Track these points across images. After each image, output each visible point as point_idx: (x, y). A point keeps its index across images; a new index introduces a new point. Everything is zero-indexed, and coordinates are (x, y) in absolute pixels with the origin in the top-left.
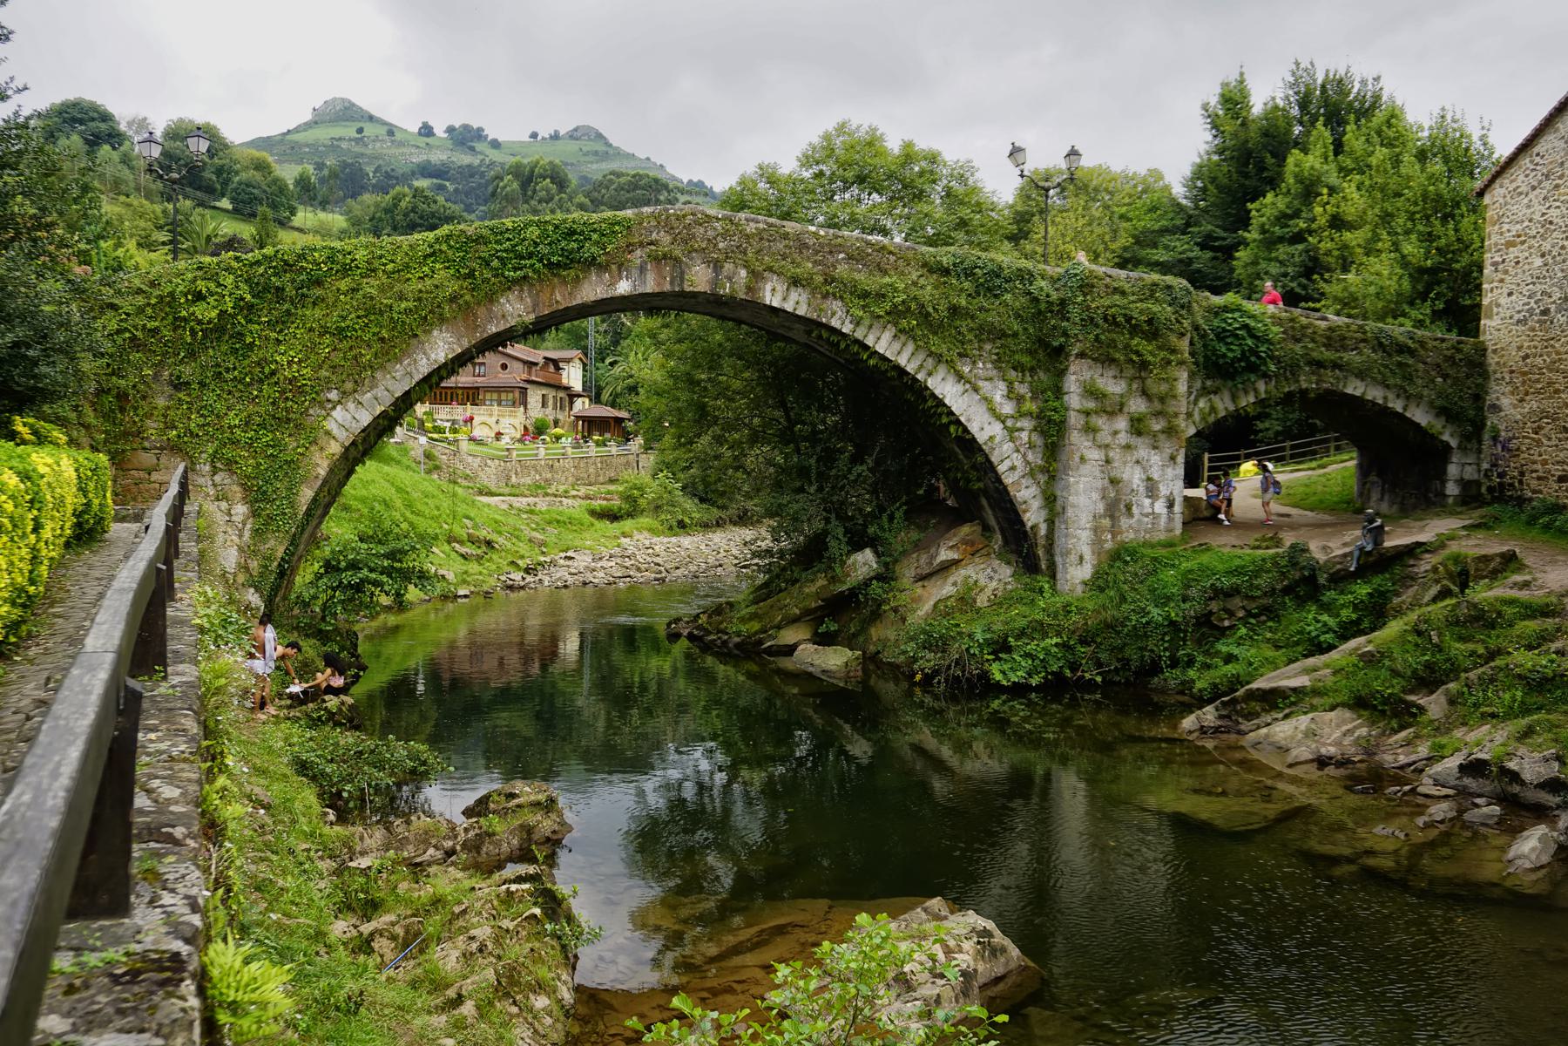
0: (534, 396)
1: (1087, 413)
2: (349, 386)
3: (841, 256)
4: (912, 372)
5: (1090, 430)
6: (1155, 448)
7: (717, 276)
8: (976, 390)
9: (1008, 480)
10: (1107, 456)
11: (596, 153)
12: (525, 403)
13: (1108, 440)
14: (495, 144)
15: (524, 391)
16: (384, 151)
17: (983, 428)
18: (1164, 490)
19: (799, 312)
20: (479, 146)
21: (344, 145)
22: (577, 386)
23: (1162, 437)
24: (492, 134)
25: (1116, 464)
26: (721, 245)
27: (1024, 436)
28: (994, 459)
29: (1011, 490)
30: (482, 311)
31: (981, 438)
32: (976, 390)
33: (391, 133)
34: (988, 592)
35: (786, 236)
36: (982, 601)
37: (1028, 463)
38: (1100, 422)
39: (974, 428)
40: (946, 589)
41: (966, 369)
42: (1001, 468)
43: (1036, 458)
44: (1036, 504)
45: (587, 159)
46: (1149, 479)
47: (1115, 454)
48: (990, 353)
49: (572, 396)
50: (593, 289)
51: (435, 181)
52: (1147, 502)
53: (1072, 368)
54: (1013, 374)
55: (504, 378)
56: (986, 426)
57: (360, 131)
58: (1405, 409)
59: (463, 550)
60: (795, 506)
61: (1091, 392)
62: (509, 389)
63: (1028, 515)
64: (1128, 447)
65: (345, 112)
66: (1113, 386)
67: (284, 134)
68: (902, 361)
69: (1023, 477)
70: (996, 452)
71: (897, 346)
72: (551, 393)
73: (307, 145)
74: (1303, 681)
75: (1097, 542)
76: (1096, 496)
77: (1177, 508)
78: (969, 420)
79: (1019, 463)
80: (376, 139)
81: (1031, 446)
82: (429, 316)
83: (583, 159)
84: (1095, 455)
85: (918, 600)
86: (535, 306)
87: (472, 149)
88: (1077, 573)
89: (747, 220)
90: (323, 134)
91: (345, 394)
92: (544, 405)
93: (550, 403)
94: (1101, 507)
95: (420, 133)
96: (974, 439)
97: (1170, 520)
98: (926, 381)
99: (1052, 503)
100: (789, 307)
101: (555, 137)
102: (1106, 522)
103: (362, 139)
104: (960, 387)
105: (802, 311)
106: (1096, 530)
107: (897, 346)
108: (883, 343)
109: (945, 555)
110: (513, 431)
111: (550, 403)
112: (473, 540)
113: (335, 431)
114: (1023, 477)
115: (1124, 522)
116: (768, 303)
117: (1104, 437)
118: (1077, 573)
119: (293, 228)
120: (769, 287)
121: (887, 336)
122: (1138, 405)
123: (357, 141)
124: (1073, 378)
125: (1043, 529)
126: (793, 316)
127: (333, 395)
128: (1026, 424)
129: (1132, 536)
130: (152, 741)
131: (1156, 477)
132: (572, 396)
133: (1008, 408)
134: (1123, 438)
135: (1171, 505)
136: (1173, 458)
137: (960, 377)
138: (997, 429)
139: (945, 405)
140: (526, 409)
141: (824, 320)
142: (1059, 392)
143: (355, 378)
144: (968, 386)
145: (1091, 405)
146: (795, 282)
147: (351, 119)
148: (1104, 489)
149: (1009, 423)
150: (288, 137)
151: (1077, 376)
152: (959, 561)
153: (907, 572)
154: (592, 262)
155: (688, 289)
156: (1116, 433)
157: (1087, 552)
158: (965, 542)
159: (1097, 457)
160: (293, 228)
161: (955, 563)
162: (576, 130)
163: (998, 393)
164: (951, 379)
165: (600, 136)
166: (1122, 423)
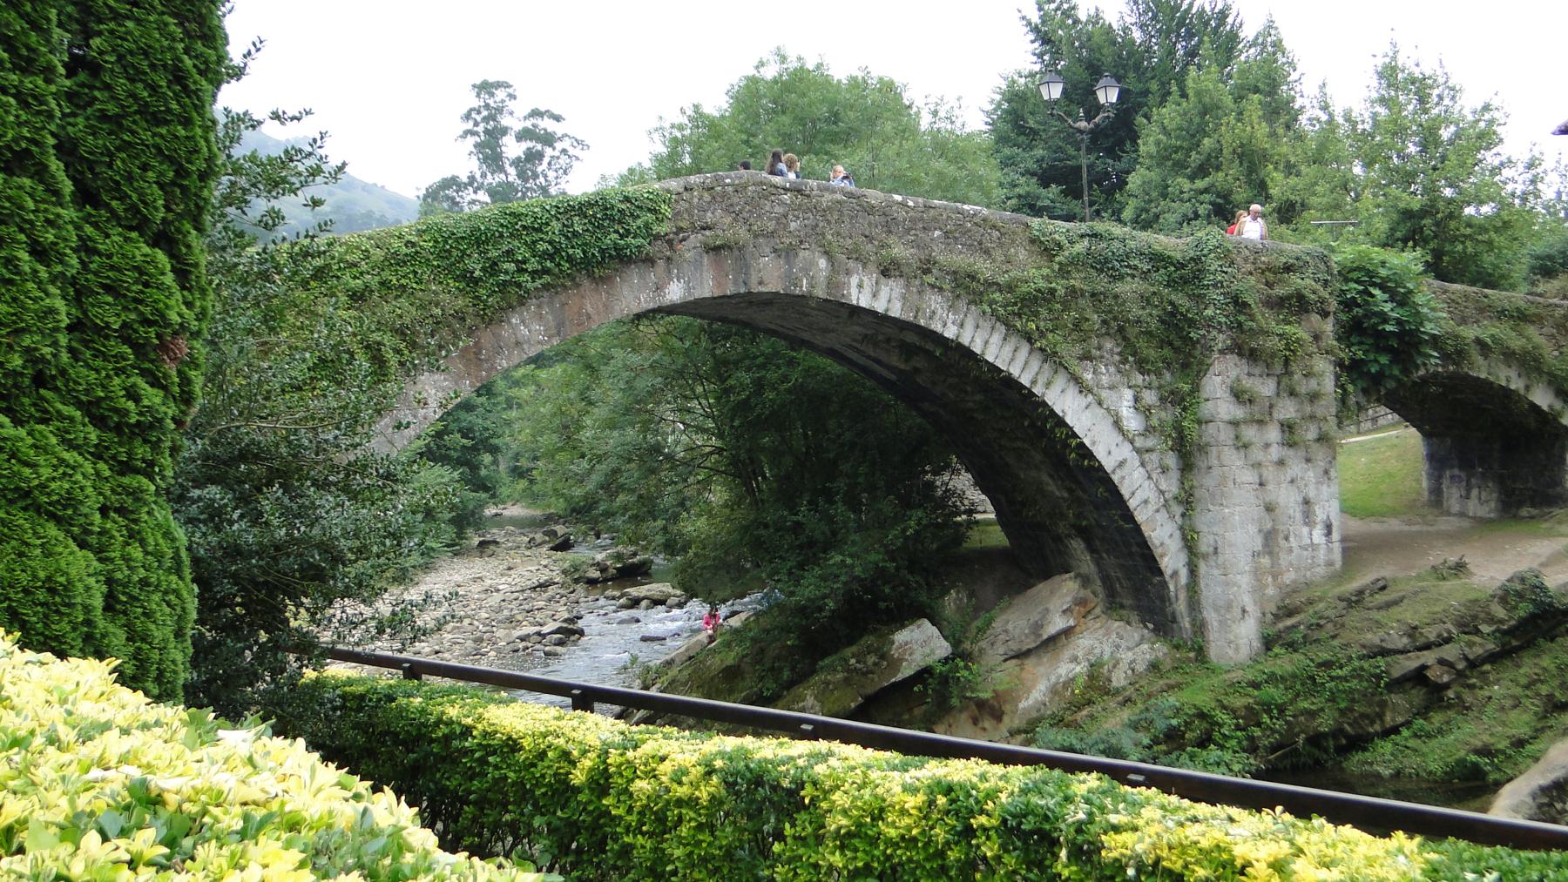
1: (1235, 424)
3: (937, 233)
4: (1028, 385)
6: (1308, 460)
7: (791, 268)
9: (1140, 517)
10: (1261, 477)
17: (1108, 449)
18: (1320, 514)
19: (893, 314)
23: (1315, 446)
25: (1270, 487)
26: (793, 226)
28: (1125, 492)
29: (1145, 529)
31: (1108, 464)
34: (1123, 666)
35: (870, 210)
37: (1162, 492)
38: (1249, 433)
39: (1100, 453)
40: (1068, 667)
42: (1132, 504)
43: (1171, 485)
47: (1269, 473)
48: (1111, 352)
52: (1305, 530)
53: (1217, 367)
56: (1113, 448)
58: (1527, 388)
60: (349, 543)
63: (1166, 559)
64: (1281, 463)
68: (1015, 371)
69: (1158, 511)
70: (1126, 482)
71: (1008, 350)
75: (1258, 589)
76: (1253, 529)
78: (1094, 443)
81: (1164, 470)
84: (1249, 476)
86: (560, 326)
89: (819, 189)
94: (1258, 543)
96: (1101, 468)
97: (1330, 550)
98: (1044, 394)
104: (1083, 401)
105: (896, 311)
106: (1257, 573)
107: (1008, 350)
114: (1158, 511)
115: (1284, 559)
116: (855, 302)
120: (854, 280)
121: (996, 339)
124: (1218, 379)
126: (884, 319)
131: (1312, 494)
133: (1133, 422)
134: (1275, 452)
135: (1329, 529)
137: (1083, 388)
138: (1126, 451)
139: (1066, 425)
141: (922, 322)
144: (1090, 397)
148: (1260, 520)
149: (1139, 442)
153: (992, 653)
155: (756, 289)
156: (1267, 446)
157: (1247, 601)
159: (1250, 479)
161: (1067, 632)
164: (1072, 391)
166: (1273, 434)
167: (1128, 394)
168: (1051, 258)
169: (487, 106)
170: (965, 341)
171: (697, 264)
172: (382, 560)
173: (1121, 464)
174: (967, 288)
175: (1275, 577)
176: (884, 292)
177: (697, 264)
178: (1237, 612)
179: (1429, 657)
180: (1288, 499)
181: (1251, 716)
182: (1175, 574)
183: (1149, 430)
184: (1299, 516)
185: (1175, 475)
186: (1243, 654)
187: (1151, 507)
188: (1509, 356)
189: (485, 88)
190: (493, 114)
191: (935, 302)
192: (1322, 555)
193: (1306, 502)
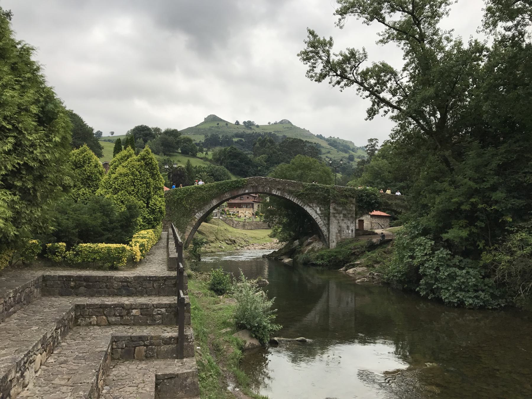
1: (334, 213)
2: (199, 210)
5: (334, 217)
11: (288, 128)
14: (258, 126)
15: (253, 204)
16: (225, 130)
17: (314, 215)
18: (351, 228)
20: (252, 127)
21: (213, 128)
24: (257, 123)
30: (222, 196)
33: (227, 124)
34: (317, 248)
35: (276, 181)
36: (316, 250)
38: (337, 215)
41: (311, 205)
43: (326, 222)
44: (326, 231)
47: (340, 221)
50: (241, 192)
51: (240, 139)
52: (347, 231)
55: (248, 201)
57: (218, 124)
59: (227, 242)
62: (249, 204)
64: (343, 220)
65: (213, 119)
67: (196, 126)
73: (203, 129)
74: (359, 262)
75: (337, 238)
77: (354, 232)
80: (223, 127)
81: (325, 220)
82: (212, 198)
84: (336, 221)
85: (305, 250)
87: (251, 128)
88: (333, 245)
90: (207, 126)
94: (337, 232)
95: (235, 124)
97: (352, 234)
99: (329, 231)
100: (277, 194)
101: (276, 123)
105: (279, 195)
106: (337, 236)
107: (298, 201)
108: (295, 201)
109: (309, 241)
110: (249, 214)
112: (230, 240)
113: (197, 217)
115: (342, 235)
117: (338, 218)
118: (333, 245)
119: (197, 157)
123: (217, 127)
133: (319, 212)
134: (342, 218)
135: (352, 231)
136: (352, 222)
137: (310, 207)
138: (318, 216)
140: (253, 208)
142: (329, 209)
143: (200, 209)
146: (279, 189)
147: (216, 121)
154: (241, 187)
158: (314, 238)
160: (197, 157)
162: (282, 121)
165: (289, 122)
166: (342, 215)
167: (318, 208)
168: (304, 188)
169: (372, 144)
170: (290, 199)
171: (250, 188)
172: (160, 199)
173: (317, 218)
174: (290, 193)
175: (340, 237)
176: (278, 192)
177: (250, 188)
178: (332, 241)
179: (356, 251)
180: (344, 225)
181: (330, 257)
182: (326, 235)
183: (321, 214)
184: (346, 228)
185: (327, 220)
186: (333, 247)
187: (322, 225)
188: (401, 207)
189: (371, 140)
190: (373, 146)
191: (286, 194)
192: (350, 235)
193: (348, 226)
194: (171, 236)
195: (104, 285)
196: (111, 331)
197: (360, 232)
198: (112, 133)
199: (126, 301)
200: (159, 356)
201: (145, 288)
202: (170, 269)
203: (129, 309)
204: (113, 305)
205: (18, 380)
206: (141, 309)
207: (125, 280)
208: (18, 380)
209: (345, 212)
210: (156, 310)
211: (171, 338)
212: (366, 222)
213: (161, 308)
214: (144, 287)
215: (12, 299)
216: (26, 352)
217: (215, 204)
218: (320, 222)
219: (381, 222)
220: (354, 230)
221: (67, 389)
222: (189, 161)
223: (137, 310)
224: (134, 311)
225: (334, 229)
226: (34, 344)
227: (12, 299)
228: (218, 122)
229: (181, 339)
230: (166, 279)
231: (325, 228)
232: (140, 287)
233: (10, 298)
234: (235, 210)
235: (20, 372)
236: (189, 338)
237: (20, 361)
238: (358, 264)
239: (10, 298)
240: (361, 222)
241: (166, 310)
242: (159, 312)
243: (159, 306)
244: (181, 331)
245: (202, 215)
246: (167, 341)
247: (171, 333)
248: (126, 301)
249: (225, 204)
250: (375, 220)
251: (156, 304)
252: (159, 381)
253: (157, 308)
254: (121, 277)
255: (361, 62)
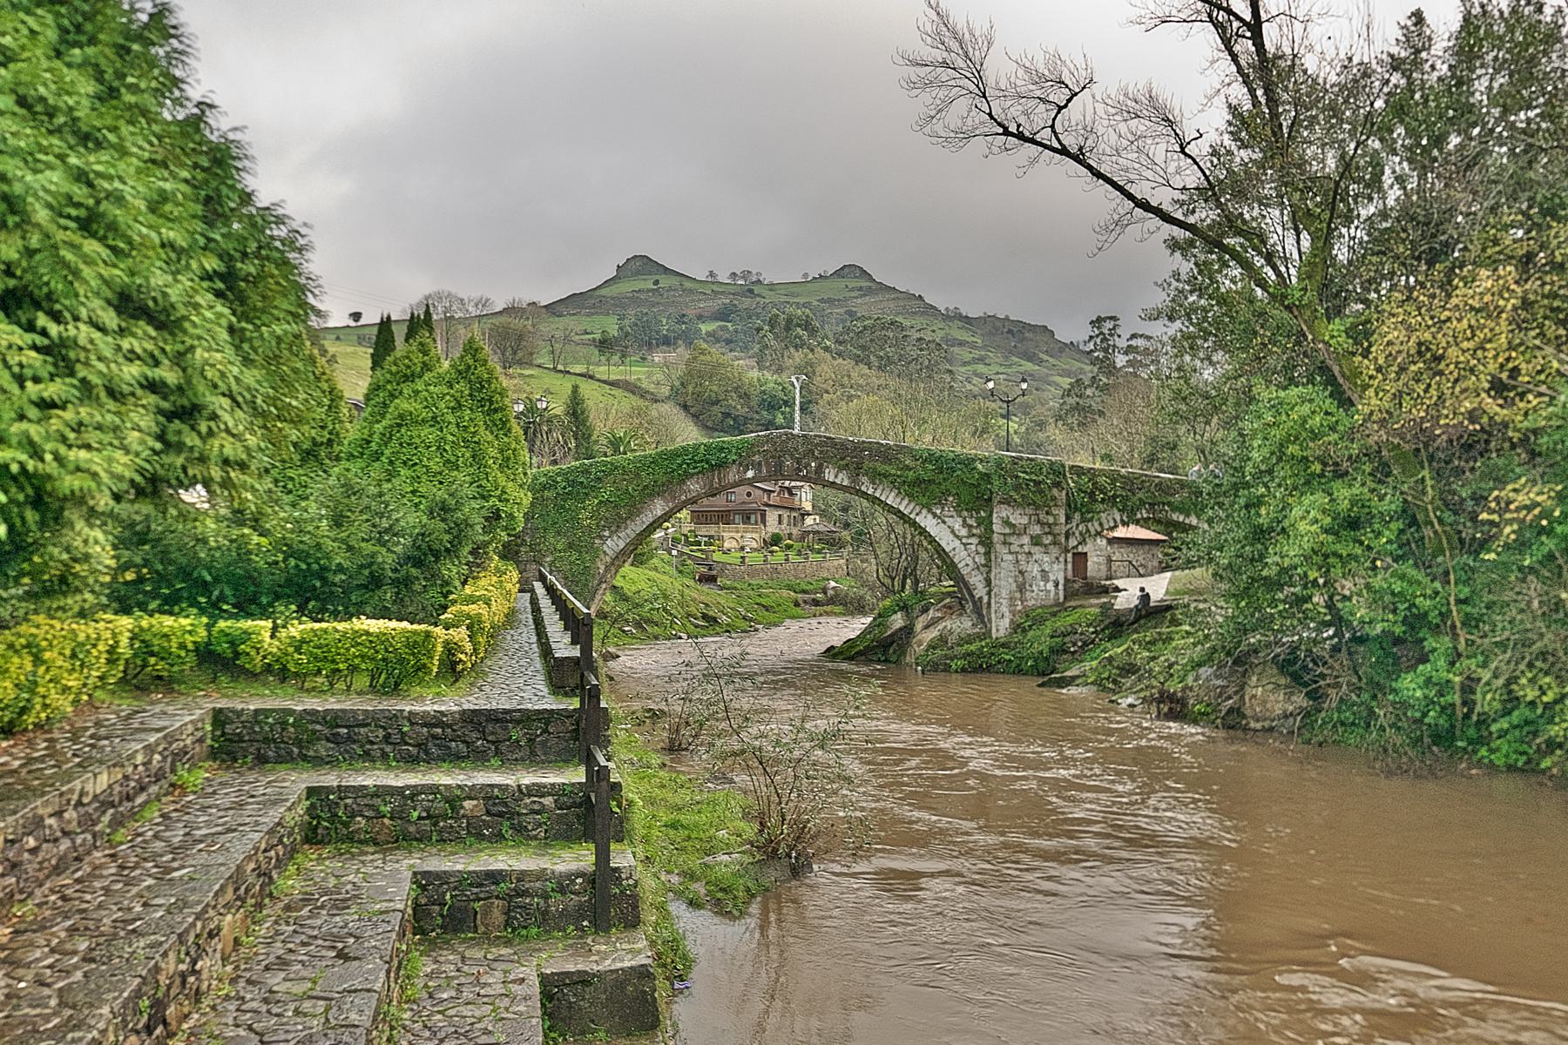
0: (772, 517)
8: (944, 522)
11: (860, 289)
12: (764, 522)
13: (1018, 549)
14: (772, 287)
17: (947, 542)
18: (1052, 577)
22: (808, 506)
24: (768, 278)
27: (973, 547)
32: (944, 522)
41: (938, 512)
43: (980, 560)
45: (853, 294)
46: (1043, 571)
49: (804, 514)
52: (1042, 583)
54: (965, 513)
57: (656, 282)
61: (1007, 523)
66: (1018, 519)
72: (785, 514)
77: (1061, 587)
79: (970, 562)
82: (650, 493)
83: (847, 295)
88: (1001, 626)
91: (612, 533)
92: (780, 522)
93: (785, 521)
97: (1057, 594)
100: (838, 481)
102: (1018, 595)
103: (657, 290)
104: (935, 521)
111: (785, 521)
122: (1037, 530)
125: (985, 599)
127: (607, 533)
128: (974, 540)
129: (1033, 602)
130: (613, 377)
132: (804, 514)
133: (964, 532)
135: (1057, 585)
137: (935, 515)
138: (957, 543)
143: (618, 524)
145: (1007, 531)
149: (964, 541)
150: (597, 293)
151: (1001, 513)
152: (942, 618)
163: (957, 524)
164: (930, 516)
165: (864, 274)
176: (840, 475)
182: (981, 598)
186: (1002, 633)
187: (969, 569)
194: (545, 603)
195: (381, 733)
196: (407, 864)
197: (1082, 586)
198: (356, 316)
199: (444, 777)
200: (547, 922)
201: (493, 742)
202: (557, 688)
203: (453, 799)
204: (408, 787)
205: (184, 983)
206: (486, 799)
207: (436, 721)
208: (184, 983)
209: (1037, 530)
210: (528, 801)
211: (571, 876)
212: (1095, 559)
213: (541, 797)
214: (490, 738)
215: (141, 768)
216: (199, 908)
217: (659, 513)
218: (965, 556)
219: (1138, 556)
220: (1062, 582)
221: (314, 1006)
222: (575, 389)
223: (475, 802)
224: (468, 804)
225: (1005, 583)
226: (217, 887)
227: (141, 768)
228: (657, 277)
229: (603, 877)
230: (547, 717)
231: (980, 577)
232: (478, 739)
233: (136, 767)
234: (712, 530)
235: (188, 959)
236: (623, 876)
237: (187, 931)
238: (1074, 678)
239: (136, 767)
240: (1081, 558)
241: (556, 801)
242: (536, 807)
243: (538, 790)
244: (603, 856)
245: (622, 545)
246: (563, 884)
247: (576, 859)
248: (444, 777)
249: (684, 514)
250: (1118, 554)
251: (527, 786)
252: (554, 991)
253: (530, 796)
254: (424, 712)
255: (1076, 94)
